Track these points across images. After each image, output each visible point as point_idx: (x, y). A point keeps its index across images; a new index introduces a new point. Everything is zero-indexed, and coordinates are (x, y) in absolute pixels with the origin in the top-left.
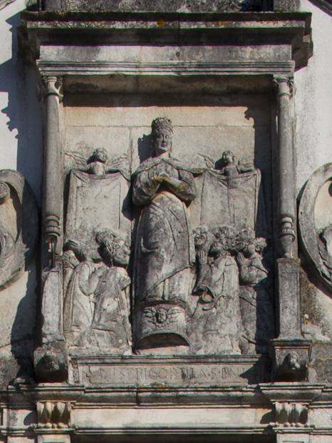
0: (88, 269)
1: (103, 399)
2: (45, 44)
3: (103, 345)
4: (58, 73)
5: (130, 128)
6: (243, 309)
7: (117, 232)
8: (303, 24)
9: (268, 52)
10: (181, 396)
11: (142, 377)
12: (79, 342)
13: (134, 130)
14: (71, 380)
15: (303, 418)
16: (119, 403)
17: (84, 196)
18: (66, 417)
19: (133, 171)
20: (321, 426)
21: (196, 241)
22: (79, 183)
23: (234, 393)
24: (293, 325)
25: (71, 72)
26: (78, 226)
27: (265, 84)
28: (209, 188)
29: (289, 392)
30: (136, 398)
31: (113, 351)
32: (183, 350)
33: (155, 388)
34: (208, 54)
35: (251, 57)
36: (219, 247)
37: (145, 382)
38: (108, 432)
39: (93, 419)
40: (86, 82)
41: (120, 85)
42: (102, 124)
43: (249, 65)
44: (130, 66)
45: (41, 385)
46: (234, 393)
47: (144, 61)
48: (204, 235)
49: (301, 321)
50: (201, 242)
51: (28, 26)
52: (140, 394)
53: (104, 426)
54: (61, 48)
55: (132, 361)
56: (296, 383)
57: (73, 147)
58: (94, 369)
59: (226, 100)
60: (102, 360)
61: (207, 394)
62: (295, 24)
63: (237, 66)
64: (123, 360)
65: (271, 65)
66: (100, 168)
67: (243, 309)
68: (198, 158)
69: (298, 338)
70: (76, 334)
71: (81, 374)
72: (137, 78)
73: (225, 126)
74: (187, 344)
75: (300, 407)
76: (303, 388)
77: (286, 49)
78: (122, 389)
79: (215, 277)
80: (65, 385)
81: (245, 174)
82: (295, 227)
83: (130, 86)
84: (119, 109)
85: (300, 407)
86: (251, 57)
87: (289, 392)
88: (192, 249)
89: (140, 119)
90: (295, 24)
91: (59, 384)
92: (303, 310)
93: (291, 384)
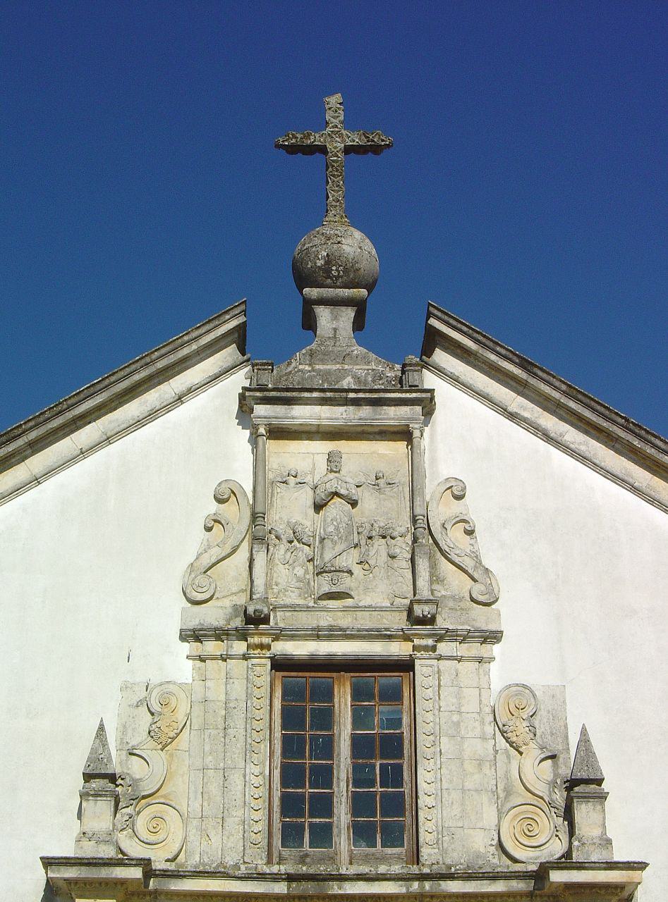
0: (283, 547)
1: (293, 636)
2: (257, 404)
3: (293, 598)
4: (266, 423)
5: (313, 454)
6: (355, 900)
7: (304, 522)
8: (429, 395)
9: (404, 411)
10: (348, 634)
11: (325, 620)
12: (277, 596)
13: (316, 456)
14: (272, 622)
15: (434, 649)
16: (305, 637)
17: (282, 498)
18: (268, 647)
19: (315, 482)
20: (446, 655)
21: (358, 529)
22: (279, 490)
23: (385, 632)
24: (425, 588)
25: (274, 422)
26: (277, 518)
27: (405, 428)
28: (367, 494)
29: (423, 632)
30: (317, 634)
31: (301, 602)
32: (349, 602)
33: (331, 628)
34: (366, 411)
35: (393, 415)
36: (374, 533)
37: (323, 623)
38: (296, 658)
39: (287, 648)
40: (284, 426)
41: (307, 429)
42: (295, 451)
43: (393, 419)
44: (313, 419)
45: (261, 626)
46: (385, 632)
47: (323, 415)
48: (363, 525)
49: (431, 582)
50: (360, 530)
51: (247, 394)
52: (320, 633)
53: (294, 653)
54: (269, 406)
55: (314, 609)
56: (428, 627)
57: (275, 466)
58: (288, 614)
59: (377, 437)
60: (294, 608)
61: (366, 633)
62: (424, 395)
63: (385, 419)
64: (308, 609)
65: (408, 419)
66: (292, 480)
67: (355, 900)
68: (359, 474)
69: (429, 598)
70: (275, 591)
71: (278, 617)
72: (319, 425)
73: (378, 454)
74: (353, 598)
75: (430, 642)
76: (434, 629)
77: (418, 409)
78: (307, 630)
79: (372, 553)
80: (267, 626)
81: (391, 486)
82: (426, 522)
83: (314, 429)
84: (306, 442)
85: (430, 642)
86: (393, 415)
87: (423, 632)
88: (356, 534)
89: (321, 448)
90: (424, 395)
91: (264, 626)
92: (432, 575)
93: (424, 627)
